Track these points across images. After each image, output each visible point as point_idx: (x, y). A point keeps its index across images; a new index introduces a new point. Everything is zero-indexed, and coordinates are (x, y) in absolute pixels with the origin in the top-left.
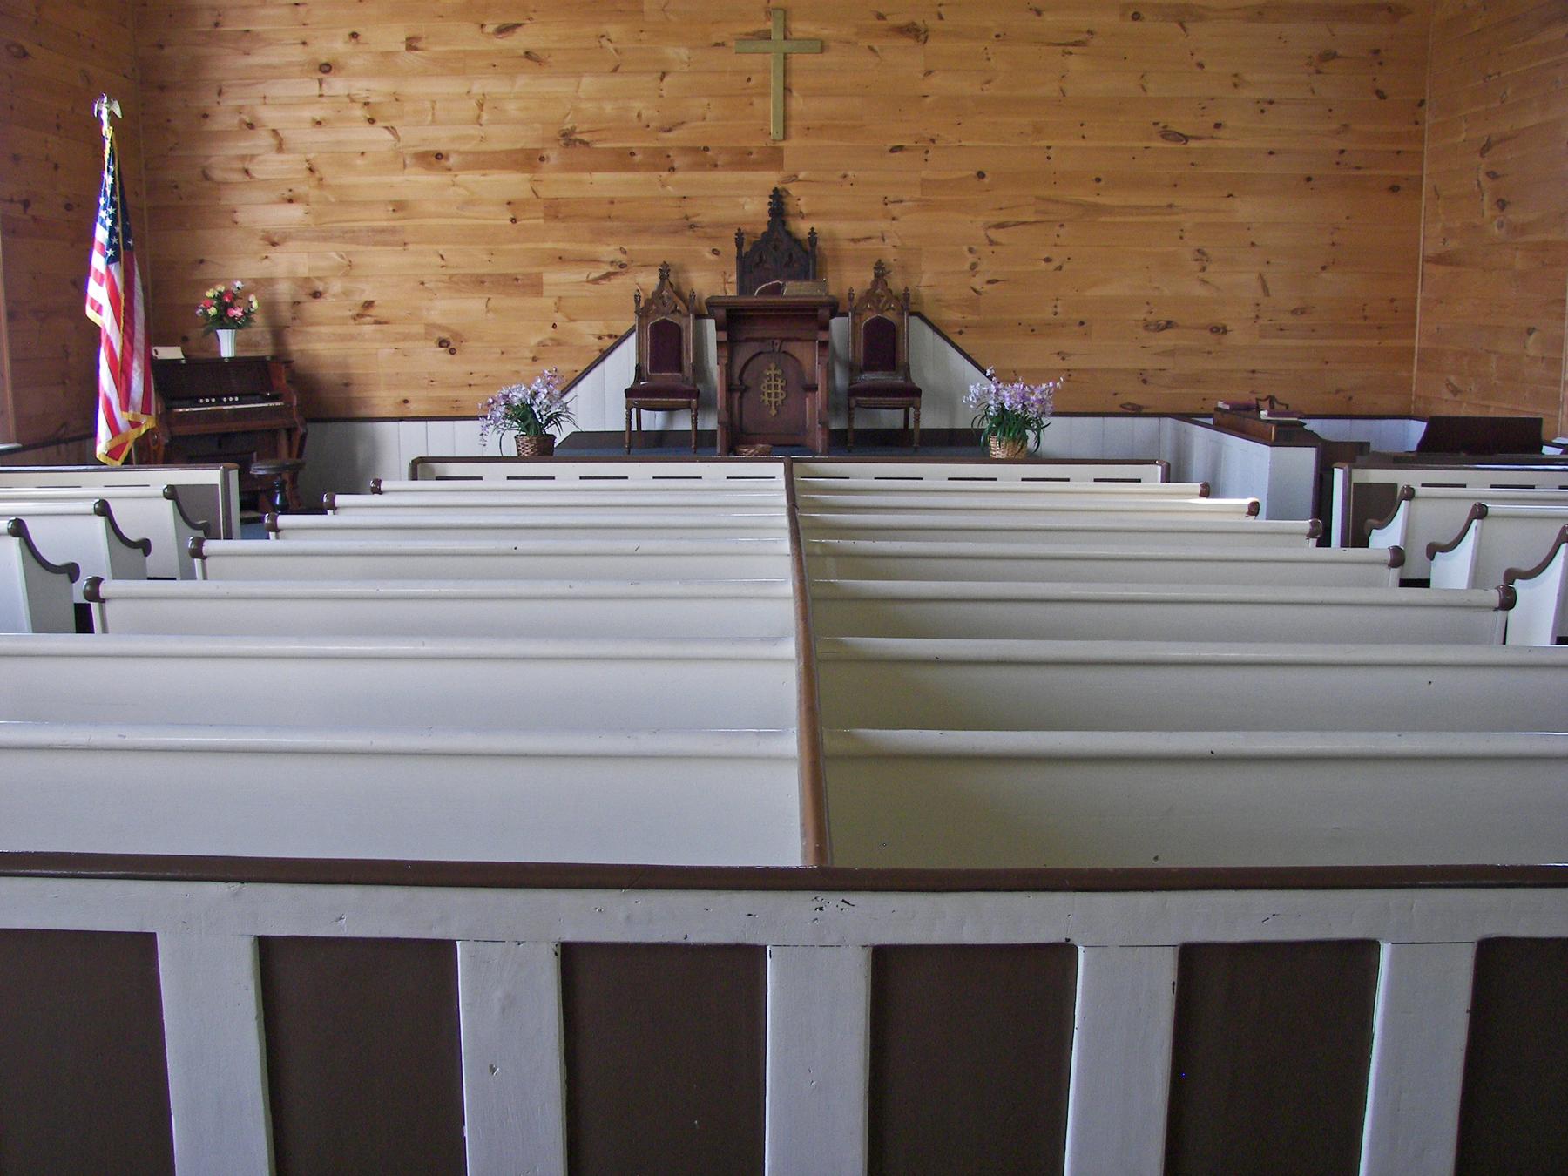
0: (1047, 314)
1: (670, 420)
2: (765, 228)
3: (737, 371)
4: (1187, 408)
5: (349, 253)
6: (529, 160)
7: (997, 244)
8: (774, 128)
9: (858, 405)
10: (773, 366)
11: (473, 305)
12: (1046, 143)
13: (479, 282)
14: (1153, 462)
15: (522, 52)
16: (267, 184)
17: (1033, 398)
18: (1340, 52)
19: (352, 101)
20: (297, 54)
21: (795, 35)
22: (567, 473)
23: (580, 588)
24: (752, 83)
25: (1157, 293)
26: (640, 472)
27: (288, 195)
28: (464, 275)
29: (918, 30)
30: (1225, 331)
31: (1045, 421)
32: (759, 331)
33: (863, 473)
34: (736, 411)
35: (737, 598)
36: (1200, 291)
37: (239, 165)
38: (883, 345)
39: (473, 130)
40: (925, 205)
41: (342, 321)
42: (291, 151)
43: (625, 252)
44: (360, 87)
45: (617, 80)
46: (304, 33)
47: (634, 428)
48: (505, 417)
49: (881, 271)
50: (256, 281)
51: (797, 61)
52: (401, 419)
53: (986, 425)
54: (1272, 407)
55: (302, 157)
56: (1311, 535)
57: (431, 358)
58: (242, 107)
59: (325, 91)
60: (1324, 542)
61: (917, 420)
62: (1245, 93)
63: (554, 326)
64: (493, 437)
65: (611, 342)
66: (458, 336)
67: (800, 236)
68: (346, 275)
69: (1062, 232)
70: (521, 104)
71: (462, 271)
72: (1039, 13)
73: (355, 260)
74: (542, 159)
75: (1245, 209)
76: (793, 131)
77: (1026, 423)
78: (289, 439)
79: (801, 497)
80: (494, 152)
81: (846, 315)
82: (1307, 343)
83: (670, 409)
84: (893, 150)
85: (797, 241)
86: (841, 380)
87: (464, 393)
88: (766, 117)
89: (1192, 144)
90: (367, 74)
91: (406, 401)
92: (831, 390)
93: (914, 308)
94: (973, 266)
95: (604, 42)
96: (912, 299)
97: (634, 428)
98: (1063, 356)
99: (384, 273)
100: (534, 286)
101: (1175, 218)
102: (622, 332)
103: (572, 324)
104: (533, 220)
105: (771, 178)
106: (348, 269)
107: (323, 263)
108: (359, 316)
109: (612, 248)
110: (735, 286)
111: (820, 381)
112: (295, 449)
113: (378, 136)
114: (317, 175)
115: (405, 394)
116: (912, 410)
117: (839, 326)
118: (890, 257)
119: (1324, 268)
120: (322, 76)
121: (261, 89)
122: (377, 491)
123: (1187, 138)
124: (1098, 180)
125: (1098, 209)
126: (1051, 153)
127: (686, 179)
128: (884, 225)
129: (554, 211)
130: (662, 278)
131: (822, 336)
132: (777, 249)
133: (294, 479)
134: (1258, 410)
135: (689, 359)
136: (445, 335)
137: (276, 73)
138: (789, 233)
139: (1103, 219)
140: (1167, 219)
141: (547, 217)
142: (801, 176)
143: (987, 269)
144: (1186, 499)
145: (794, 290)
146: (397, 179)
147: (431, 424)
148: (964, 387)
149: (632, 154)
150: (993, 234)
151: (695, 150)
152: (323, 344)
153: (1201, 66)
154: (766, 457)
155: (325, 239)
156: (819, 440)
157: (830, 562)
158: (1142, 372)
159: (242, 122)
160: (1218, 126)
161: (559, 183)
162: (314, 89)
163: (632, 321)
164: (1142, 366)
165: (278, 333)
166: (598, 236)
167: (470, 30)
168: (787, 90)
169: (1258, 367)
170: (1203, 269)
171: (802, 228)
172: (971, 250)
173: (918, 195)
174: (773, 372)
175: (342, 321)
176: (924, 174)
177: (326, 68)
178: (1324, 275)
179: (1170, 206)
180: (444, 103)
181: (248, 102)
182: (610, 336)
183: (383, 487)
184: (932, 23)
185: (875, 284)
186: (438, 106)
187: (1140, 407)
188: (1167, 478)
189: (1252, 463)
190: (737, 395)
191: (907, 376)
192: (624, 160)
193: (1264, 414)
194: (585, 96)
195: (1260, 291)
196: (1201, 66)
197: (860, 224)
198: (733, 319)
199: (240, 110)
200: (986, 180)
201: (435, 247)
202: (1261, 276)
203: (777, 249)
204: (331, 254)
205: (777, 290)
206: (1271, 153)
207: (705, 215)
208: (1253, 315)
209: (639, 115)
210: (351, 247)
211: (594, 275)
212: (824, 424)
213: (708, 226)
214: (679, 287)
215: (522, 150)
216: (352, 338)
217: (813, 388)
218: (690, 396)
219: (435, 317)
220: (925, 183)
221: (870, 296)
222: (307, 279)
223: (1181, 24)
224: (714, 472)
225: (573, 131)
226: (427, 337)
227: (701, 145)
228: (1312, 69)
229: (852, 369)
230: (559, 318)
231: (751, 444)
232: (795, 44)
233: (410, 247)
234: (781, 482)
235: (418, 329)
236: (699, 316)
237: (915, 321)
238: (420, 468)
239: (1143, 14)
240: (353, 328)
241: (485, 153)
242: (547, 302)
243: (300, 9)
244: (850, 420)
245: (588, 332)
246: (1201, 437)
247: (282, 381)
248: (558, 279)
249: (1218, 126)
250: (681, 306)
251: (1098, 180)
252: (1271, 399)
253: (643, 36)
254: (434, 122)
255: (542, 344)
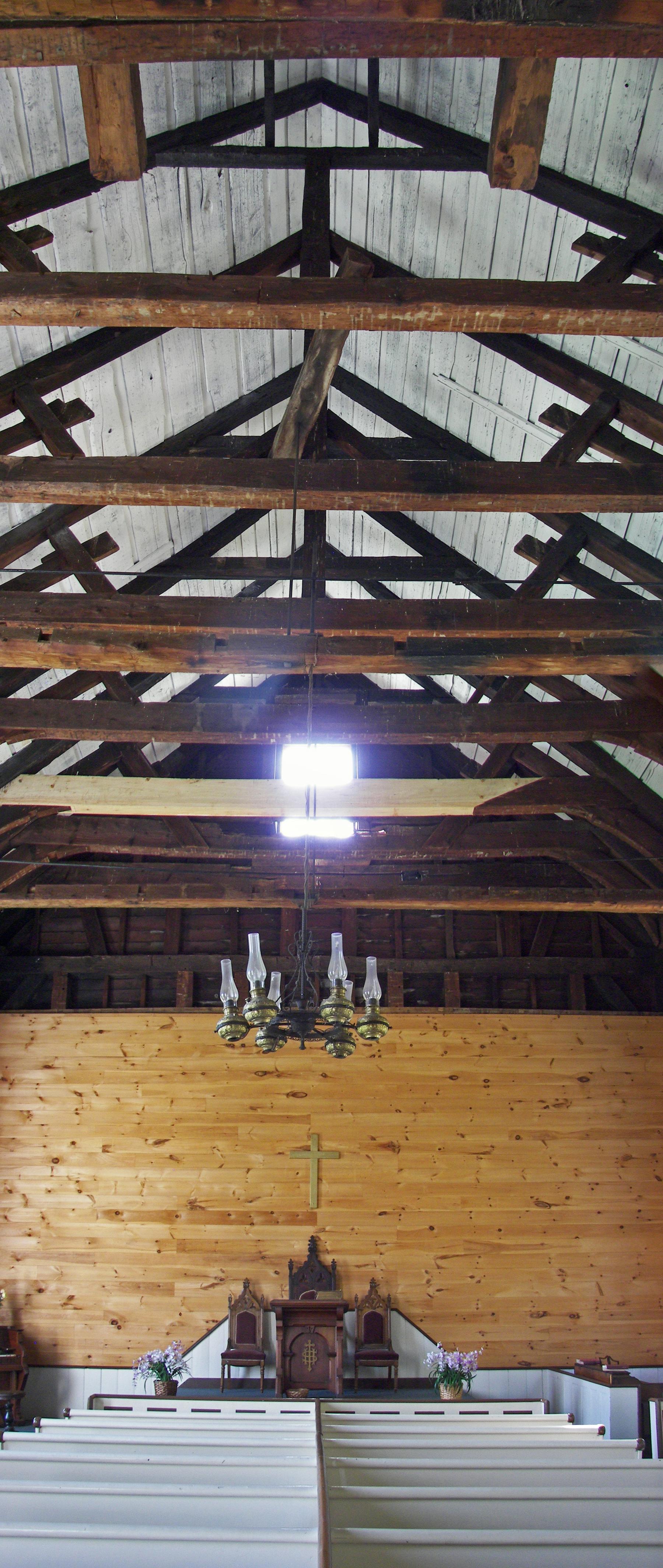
0: (472, 1309)
1: (248, 1372)
2: (306, 1259)
3: (288, 1344)
4: (558, 1364)
5: (61, 1267)
6: (170, 1217)
7: (442, 1268)
8: (312, 1202)
9: (361, 1364)
10: (309, 1341)
11: (133, 1300)
12: (470, 1209)
13: (137, 1287)
14: (538, 1400)
15: (168, 1155)
16: (17, 1225)
17: (465, 1361)
18: (634, 1155)
19: (70, 1180)
20: (40, 1152)
21: (325, 1148)
22: (183, 1406)
23: (186, 1489)
24: (300, 1175)
25: (537, 1295)
26: (228, 1407)
27: (28, 1231)
28: (129, 1283)
29: (394, 1146)
30: (578, 1317)
31: (473, 1374)
32: (302, 1320)
33: (363, 1409)
34: (287, 1366)
35: (283, 1497)
36: (562, 1294)
37: (2, 1213)
38: (375, 1328)
39: (138, 1199)
40: (400, 1246)
41: (55, 1307)
42: (32, 1207)
43: (223, 1272)
44: (75, 1172)
45: (221, 1171)
46: (45, 1141)
47: (226, 1376)
48: (149, 1368)
49: (374, 1284)
50: (5, 1281)
51: (325, 1163)
52: (86, 1367)
53: (438, 1376)
54: (609, 1363)
55: (38, 1210)
56: (638, 1449)
57: (107, 1331)
58: (6, 1180)
59: (55, 1173)
60: (647, 1454)
61: (396, 1374)
62: (582, 1179)
63: (180, 1314)
64: (140, 1381)
65: (214, 1325)
66: (123, 1318)
67: (327, 1264)
68: (59, 1280)
69: (480, 1260)
70: (166, 1185)
71: (128, 1280)
72: (463, 1136)
73: (65, 1271)
74: (177, 1216)
75: (586, 1245)
76: (322, 1203)
77: (462, 1375)
78: (18, 1377)
79: (325, 1426)
80: (149, 1212)
81: (353, 1310)
82: (628, 1322)
83: (248, 1366)
84: (381, 1214)
85: (325, 1267)
86: (350, 1349)
87: (125, 1353)
88: (307, 1195)
89: (553, 1208)
90: (80, 1165)
91: (90, 1357)
92: (345, 1355)
93: (394, 1306)
94: (428, 1281)
95: (215, 1151)
96: (392, 1301)
97: (226, 1376)
98: (482, 1333)
99: (82, 1280)
100: (170, 1291)
101: (545, 1251)
102: (220, 1319)
103: (190, 1314)
104: (171, 1252)
105: (309, 1230)
106: (61, 1276)
107: (46, 1272)
108: (65, 1304)
109: (214, 1269)
110: (288, 1293)
111: (338, 1350)
112: (20, 1387)
113: (83, 1200)
114: (46, 1221)
115: (89, 1352)
116: (393, 1367)
117: (349, 1318)
118: (379, 1276)
119: (634, 1278)
120: (53, 1165)
121: (18, 1171)
122: (67, 1415)
123: (550, 1205)
124: (500, 1230)
125: (501, 1247)
126: (472, 1215)
127: (261, 1230)
128: (376, 1257)
129: (183, 1247)
130: (245, 1287)
131: (339, 1324)
132: (313, 1272)
133: (18, 1402)
134: (601, 1365)
135: (260, 1336)
136: (115, 1318)
137: (28, 1162)
138: (320, 1262)
139: (503, 1253)
140: (541, 1252)
141: (178, 1250)
142: (327, 1228)
143: (437, 1283)
144: (560, 1423)
145: (323, 1296)
146: (92, 1225)
147: (103, 1370)
148: (425, 1355)
149: (229, 1215)
150: (440, 1262)
151: (266, 1213)
152: (41, 1321)
153: (556, 1164)
154: (305, 1398)
155: (48, 1258)
156: (337, 1386)
157: (342, 1472)
158: (530, 1343)
159: (6, 1189)
160: (567, 1198)
161: (186, 1230)
162: (48, 1172)
163: (226, 1312)
164: (529, 1339)
165: (16, 1312)
166: (208, 1261)
167: (139, 1142)
168: (319, 1179)
169: (598, 1338)
170: (564, 1281)
171: (328, 1259)
172: (427, 1272)
173: (395, 1240)
174: (310, 1345)
175: (55, 1307)
176: (399, 1228)
177: (56, 1161)
178: (634, 1282)
179: (542, 1244)
180: (121, 1183)
181: (11, 1178)
182: (213, 1321)
183: (71, 1413)
184: (403, 1142)
185: (370, 1292)
186: (119, 1183)
187: (530, 1364)
188: (548, 1411)
189: (598, 1397)
190: (288, 1358)
191: (390, 1346)
192: (224, 1218)
193: (604, 1367)
194: (203, 1181)
195: (598, 1292)
196: (556, 1164)
197: (361, 1256)
198: (287, 1314)
199: (5, 1182)
200: (435, 1231)
201: (113, 1265)
202: (598, 1284)
203: (313, 1272)
204: (51, 1267)
205: (312, 1296)
206: (599, 1213)
207: (271, 1251)
208: (594, 1307)
209: (234, 1193)
210: (64, 1264)
211: (205, 1285)
212: (340, 1376)
213: (272, 1257)
214: (254, 1292)
215: (166, 1211)
216: (59, 1317)
217: (334, 1355)
218: (262, 1359)
219: (110, 1306)
220: (399, 1233)
221: (368, 1299)
222: (36, 1281)
223: (543, 1141)
224: (273, 1408)
225: (195, 1201)
226: (104, 1318)
227: (270, 1211)
228: (618, 1165)
229: (358, 1343)
230: (183, 1309)
231: (296, 1388)
232: (324, 1154)
233: (98, 1265)
234: (313, 1416)
235: (99, 1313)
236: (266, 1310)
237: (394, 1313)
238: (95, 1401)
239: (522, 1136)
240: (61, 1312)
241: (143, 1212)
242: (176, 1300)
243: (44, 1127)
244: (356, 1373)
245: (200, 1318)
246: (567, 1382)
247: (16, 1342)
248: (183, 1286)
249: (567, 1198)
250: (256, 1304)
251: (500, 1230)
252: (608, 1358)
253: (237, 1148)
254: (115, 1193)
255: (173, 1325)
